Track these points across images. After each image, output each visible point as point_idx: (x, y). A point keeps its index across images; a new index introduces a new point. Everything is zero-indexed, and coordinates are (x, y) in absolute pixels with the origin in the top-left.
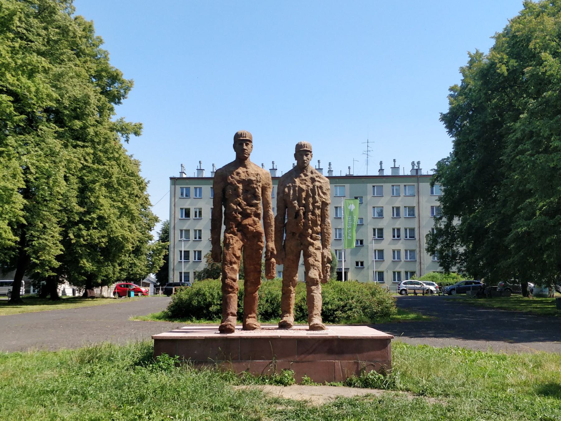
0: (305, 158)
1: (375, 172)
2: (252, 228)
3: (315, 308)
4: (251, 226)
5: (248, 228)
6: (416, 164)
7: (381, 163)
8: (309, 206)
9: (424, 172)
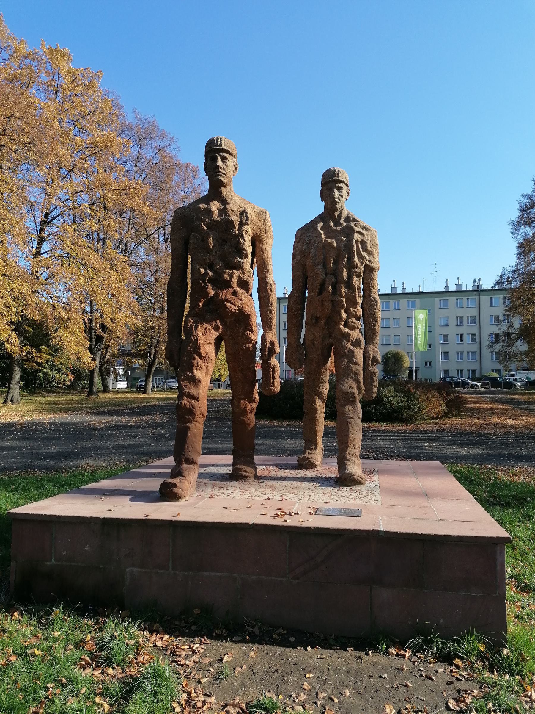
0: (336, 193)
1: (441, 288)
2: (233, 306)
3: (349, 443)
4: (232, 303)
5: (226, 306)
6: (478, 281)
7: (447, 281)
8: (342, 273)
9: (484, 287)
